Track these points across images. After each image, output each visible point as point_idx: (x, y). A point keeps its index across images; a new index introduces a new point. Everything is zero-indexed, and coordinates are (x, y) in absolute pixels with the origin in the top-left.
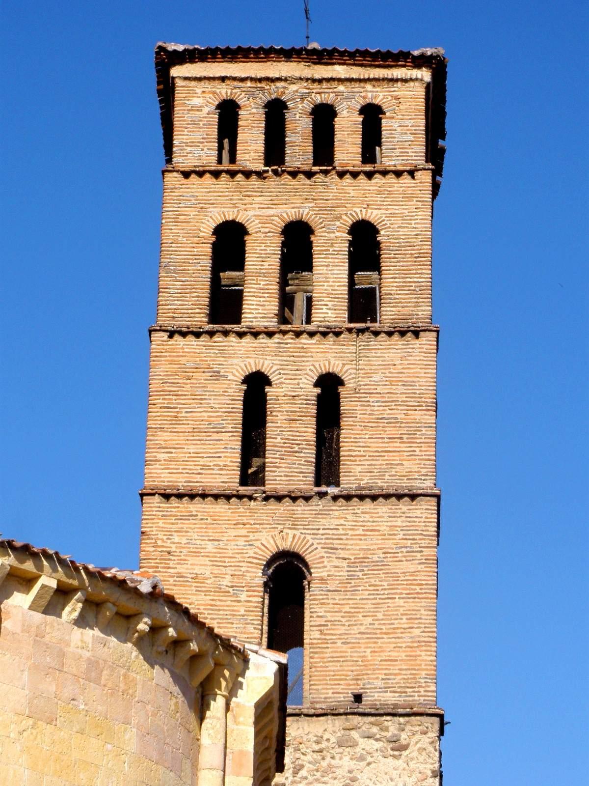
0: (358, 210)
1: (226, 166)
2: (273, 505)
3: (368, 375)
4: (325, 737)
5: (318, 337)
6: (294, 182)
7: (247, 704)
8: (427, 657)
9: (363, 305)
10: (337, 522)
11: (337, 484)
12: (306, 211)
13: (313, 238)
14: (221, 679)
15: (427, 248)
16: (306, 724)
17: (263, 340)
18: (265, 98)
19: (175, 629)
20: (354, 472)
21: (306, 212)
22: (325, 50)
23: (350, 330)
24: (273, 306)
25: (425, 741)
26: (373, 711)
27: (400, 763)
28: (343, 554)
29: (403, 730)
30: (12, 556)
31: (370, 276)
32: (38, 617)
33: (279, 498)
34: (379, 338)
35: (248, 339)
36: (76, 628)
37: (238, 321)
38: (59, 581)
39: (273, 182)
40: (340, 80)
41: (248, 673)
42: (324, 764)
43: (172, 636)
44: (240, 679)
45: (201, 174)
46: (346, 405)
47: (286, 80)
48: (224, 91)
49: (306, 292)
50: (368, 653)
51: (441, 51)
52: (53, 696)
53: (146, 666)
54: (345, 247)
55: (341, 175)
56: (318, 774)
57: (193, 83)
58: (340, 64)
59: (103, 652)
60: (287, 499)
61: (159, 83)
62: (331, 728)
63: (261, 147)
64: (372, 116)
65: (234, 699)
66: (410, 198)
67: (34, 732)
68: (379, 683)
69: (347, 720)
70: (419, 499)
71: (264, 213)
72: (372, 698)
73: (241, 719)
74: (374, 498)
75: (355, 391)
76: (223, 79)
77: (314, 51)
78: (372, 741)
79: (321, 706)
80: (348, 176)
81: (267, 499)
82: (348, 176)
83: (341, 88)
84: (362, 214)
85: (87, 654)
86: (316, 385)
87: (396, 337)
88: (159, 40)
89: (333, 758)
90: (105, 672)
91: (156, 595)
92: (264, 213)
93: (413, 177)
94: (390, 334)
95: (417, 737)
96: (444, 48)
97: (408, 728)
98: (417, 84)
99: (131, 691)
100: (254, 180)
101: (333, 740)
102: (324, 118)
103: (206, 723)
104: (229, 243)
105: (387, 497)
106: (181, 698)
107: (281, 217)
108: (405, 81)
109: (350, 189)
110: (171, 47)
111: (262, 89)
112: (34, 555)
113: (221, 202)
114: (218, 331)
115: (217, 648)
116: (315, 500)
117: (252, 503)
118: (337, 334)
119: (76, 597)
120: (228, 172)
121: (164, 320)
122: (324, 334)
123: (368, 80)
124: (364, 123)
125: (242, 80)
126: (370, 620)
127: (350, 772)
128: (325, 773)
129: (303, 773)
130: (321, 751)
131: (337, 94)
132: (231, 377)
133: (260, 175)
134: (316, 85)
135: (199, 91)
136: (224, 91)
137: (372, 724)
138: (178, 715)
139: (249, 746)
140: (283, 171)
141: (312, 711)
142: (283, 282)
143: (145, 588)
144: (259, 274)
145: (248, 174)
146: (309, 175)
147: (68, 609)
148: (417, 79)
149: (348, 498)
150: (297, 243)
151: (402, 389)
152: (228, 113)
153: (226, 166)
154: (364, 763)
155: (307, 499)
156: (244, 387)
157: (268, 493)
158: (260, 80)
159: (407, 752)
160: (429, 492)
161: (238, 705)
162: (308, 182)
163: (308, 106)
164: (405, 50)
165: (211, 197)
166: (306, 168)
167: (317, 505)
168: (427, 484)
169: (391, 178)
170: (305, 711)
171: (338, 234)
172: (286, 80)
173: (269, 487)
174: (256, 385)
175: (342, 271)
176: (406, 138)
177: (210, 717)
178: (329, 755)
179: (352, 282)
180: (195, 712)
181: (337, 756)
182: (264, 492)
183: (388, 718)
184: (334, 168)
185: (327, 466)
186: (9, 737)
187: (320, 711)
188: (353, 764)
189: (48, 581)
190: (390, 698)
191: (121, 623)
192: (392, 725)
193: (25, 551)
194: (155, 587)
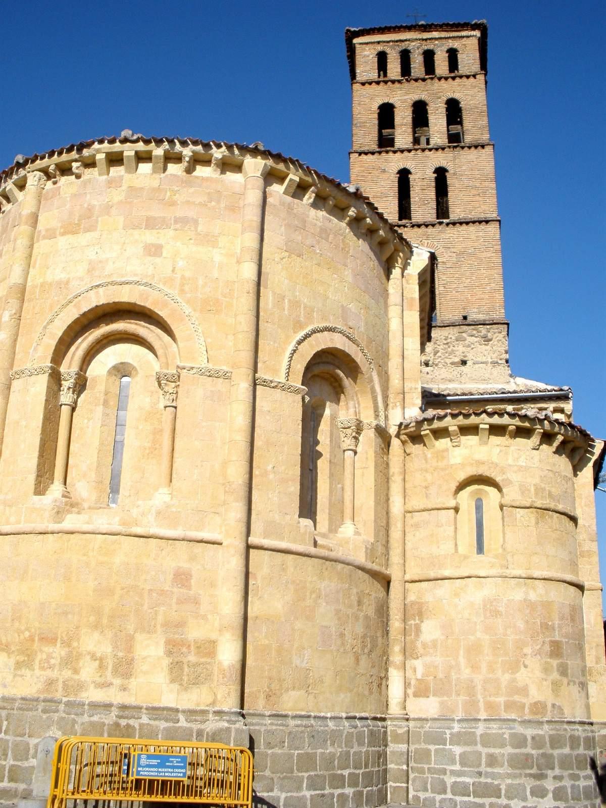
0: (449, 94)
1: (382, 78)
2: (416, 229)
3: (460, 167)
4: (449, 337)
5: (433, 151)
6: (417, 84)
7: (414, 274)
8: (500, 297)
9: (455, 139)
10: (449, 235)
11: (448, 218)
12: (423, 96)
13: (427, 107)
14: (399, 258)
15: (485, 108)
16: (439, 331)
17: (406, 153)
18: (400, 49)
19: (371, 219)
20: (456, 213)
21: (423, 96)
22: (427, 25)
23: (449, 147)
24: (410, 139)
25: (501, 336)
26: (473, 323)
27: (488, 347)
28: (453, 250)
29: (489, 332)
30: (271, 160)
31: (457, 127)
32: (289, 199)
33: (419, 226)
34: (464, 149)
35: (398, 154)
36: (312, 209)
37: (393, 146)
38: (300, 179)
39: (406, 85)
40: (436, 39)
41: (413, 258)
42: (450, 350)
43: (369, 223)
44: (409, 261)
45: (370, 83)
46: (450, 181)
47: (409, 40)
48: (379, 48)
49: (426, 136)
50: (469, 297)
51: (485, 21)
52: (300, 243)
53: (355, 238)
54: (444, 110)
55: (440, 79)
56: (447, 354)
57: (364, 46)
58: (435, 31)
59: (330, 225)
60: (423, 226)
61: (348, 52)
62: (452, 333)
63: (399, 70)
64: (453, 55)
65: (406, 271)
66: (475, 87)
67: (290, 260)
68: (476, 310)
69: (460, 328)
70: (490, 223)
71: (402, 99)
72: (472, 317)
73: (411, 282)
74: (467, 223)
75: (455, 174)
76: (379, 42)
77: (422, 25)
78: (473, 338)
79: (447, 322)
80: (443, 79)
81: (413, 226)
82: (443, 79)
83: (437, 42)
84: (451, 95)
85: (319, 224)
86: (434, 173)
87: (473, 149)
88: (346, 26)
89: (454, 346)
90: (331, 236)
91: (357, 196)
92: (402, 99)
93: (475, 78)
94: (469, 147)
95: (497, 334)
96: (486, 19)
97: (492, 330)
98: (474, 38)
99: (347, 249)
100: (397, 85)
101: (453, 338)
102: (429, 56)
103: (391, 282)
104: (386, 114)
105: (474, 222)
106: (376, 262)
107: (411, 99)
108: (468, 37)
109: (445, 85)
110: (352, 29)
111: (398, 45)
112: (285, 161)
113: (380, 95)
114: (383, 151)
115: (395, 239)
116: (437, 226)
117: (406, 229)
118: (443, 149)
119: (311, 190)
120: (383, 81)
121: (356, 147)
122: (437, 149)
123: (449, 38)
124: (449, 56)
125: (388, 42)
126: (469, 280)
127: (463, 353)
128: (450, 354)
129: (439, 354)
130: (447, 344)
131: (435, 45)
132: (391, 171)
133: (399, 82)
134: (424, 42)
135: (367, 49)
136: (379, 48)
137: (474, 329)
138: (375, 271)
139: (416, 295)
140: (411, 79)
141: (442, 325)
142: (414, 132)
143: (352, 189)
144: (402, 125)
145: (393, 82)
146: (424, 80)
147: (307, 197)
148: (473, 36)
149: (454, 224)
150: (420, 112)
151: (477, 172)
152: (382, 58)
153: (382, 78)
154: (469, 349)
155: (433, 225)
156: (398, 175)
157: (414, 223)
158: (397, 41)
159: (492, 342)
160: (495, 219)
161: (408, 274)
162: (424, 83)
163: (421, 51)
164: (467, 22)
165: (376, 93)
166: (422, 76)
167: (438, 228)
168: (494, 215)
169: (464, 79)
170: (438, 325)
171: (440, 105)
172: (409, 40)
173: (414, 220)
174: (404, 176)
175: (443, 121)
176: (469, 62)
177: (393, 279)
178: (452, 345)
179: (448, 131)
180: (384, 270)
181: (456, 346)
182: (411, 223)
183: (481, 326)
184: (436, 76)
185: (442, 210)
186: (274, 260)
187: (446, 324)
188: (464, 349)
189: (294, 176)
190: (481, 317)
191: (339, 211)
192: (483, 330)
193: (278, 157)
194: (357, 190)
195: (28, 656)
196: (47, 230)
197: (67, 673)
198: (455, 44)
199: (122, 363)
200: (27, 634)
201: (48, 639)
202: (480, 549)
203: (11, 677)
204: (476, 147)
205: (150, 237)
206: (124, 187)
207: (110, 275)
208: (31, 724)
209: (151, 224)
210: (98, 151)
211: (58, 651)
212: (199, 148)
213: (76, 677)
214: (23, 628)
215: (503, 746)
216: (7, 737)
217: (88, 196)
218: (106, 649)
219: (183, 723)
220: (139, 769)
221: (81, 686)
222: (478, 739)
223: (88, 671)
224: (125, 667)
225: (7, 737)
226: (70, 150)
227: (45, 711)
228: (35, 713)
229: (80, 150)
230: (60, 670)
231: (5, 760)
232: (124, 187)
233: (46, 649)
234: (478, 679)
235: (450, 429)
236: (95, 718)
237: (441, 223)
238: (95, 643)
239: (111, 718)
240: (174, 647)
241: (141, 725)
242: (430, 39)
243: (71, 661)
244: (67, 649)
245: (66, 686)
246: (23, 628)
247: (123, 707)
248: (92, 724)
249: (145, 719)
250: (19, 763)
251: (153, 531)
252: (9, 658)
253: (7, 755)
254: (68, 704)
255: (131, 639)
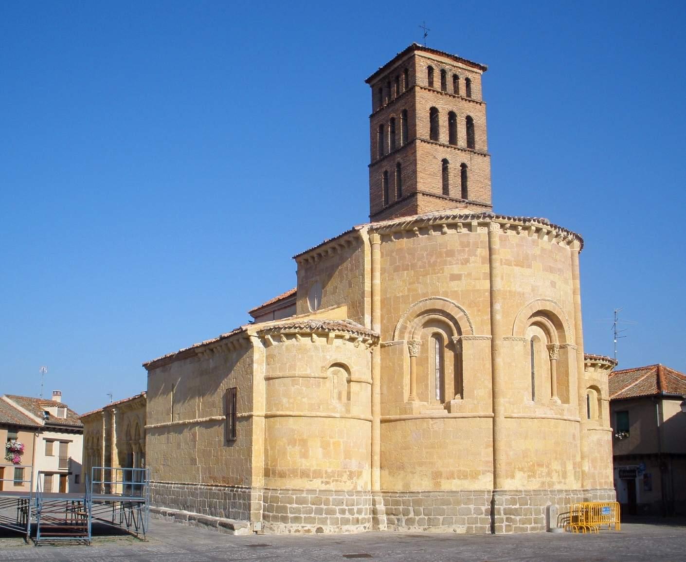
33: (453, 200)
40: (460, 68)
57: (420, 58)
74: (476, 205)
76: (429, 58)
77: (456, 57)
81: (450, 200)
86: (461, 166)
92: (444, 106)
105: (480, 205)
108: (476, 73)
110: (418, 45)
118: (465, 151)
123: (467, 70)
155: (460, 202)
158: (439, 62)
172: (446, 64)
174: (445, 162)
195: (533, 472)
196: (506, 260)
197: (548, 479)
198: (470, 76)
199: (535, 336)
200: (531, 463)
201: (540, 465)
202: (589, 417)
203: (526, 482)
204: (481, 155)
205: (552, 277)
206: (539, 247)
207: (541, 295)
208: (540, 501)
209: (551, 270)
210: (533, 225)
211: (545, 470)
212: (566, 233)
213: (552, 480)
214: (529, 460)
215: (605, 499)
216: (531, 507)
217: (525, 247)
218: (559, 468)
219: (579, 496)
220: (56, 444)
221: (553, 484)
222: (598, 497)
223: (555, 478)
224: (564, 475)
225: (531, 507)
226: (520, 220)
227: (545, 495)
228: (541, 496)
229: (525, 221)
230: (546, 478)
231: (532, 515)
232: (539, 247)
233: (540, 469)
234: (596, 472)
235: (588, 364)
236: (560, 496)
237: (464, 201)
238: (556, 466)
239: (563, 495)
240: (574, 464)
241: (572, 497)
242: (457, 67)
243: (549, 474)
244: (548, 469)
245: (549, 484)
246: (529, 460)
247: (566, 491)
248: (560, 498)
249: (572, 496)
250: (537, 517)
251: (570, 418)
252: (524, 473)
253: (532, 514)
254: (551, 491)
255: (565, 462)
